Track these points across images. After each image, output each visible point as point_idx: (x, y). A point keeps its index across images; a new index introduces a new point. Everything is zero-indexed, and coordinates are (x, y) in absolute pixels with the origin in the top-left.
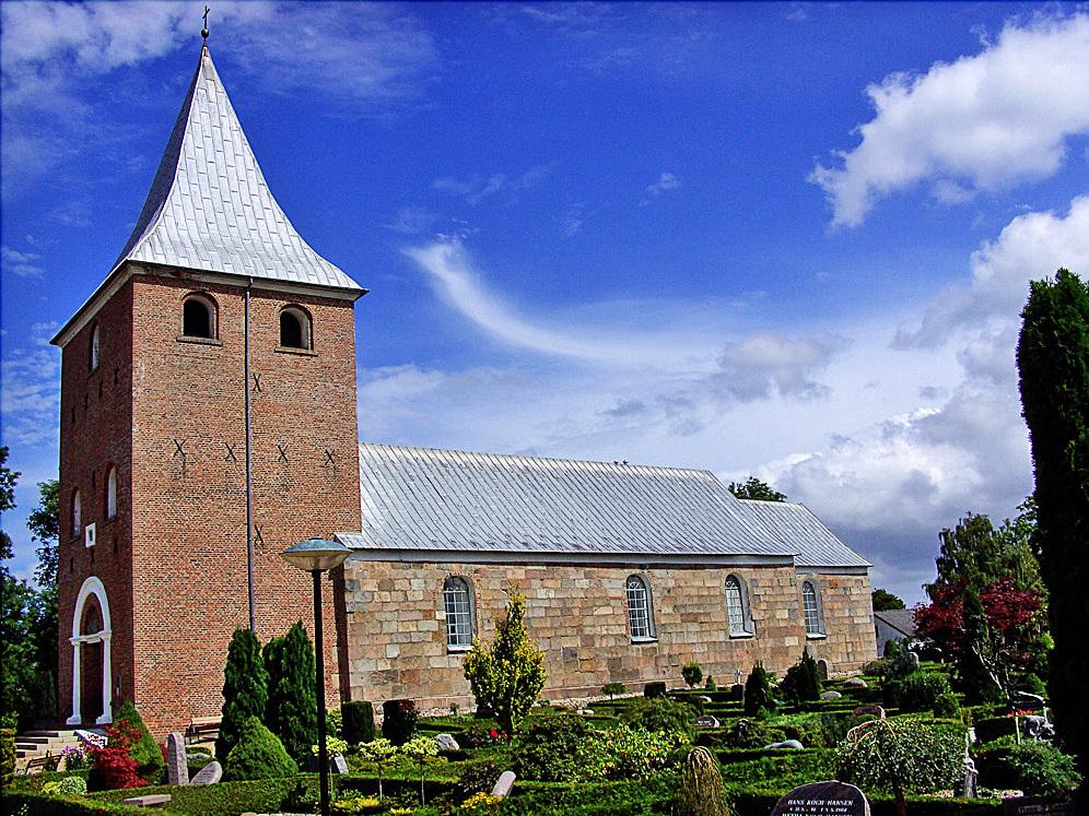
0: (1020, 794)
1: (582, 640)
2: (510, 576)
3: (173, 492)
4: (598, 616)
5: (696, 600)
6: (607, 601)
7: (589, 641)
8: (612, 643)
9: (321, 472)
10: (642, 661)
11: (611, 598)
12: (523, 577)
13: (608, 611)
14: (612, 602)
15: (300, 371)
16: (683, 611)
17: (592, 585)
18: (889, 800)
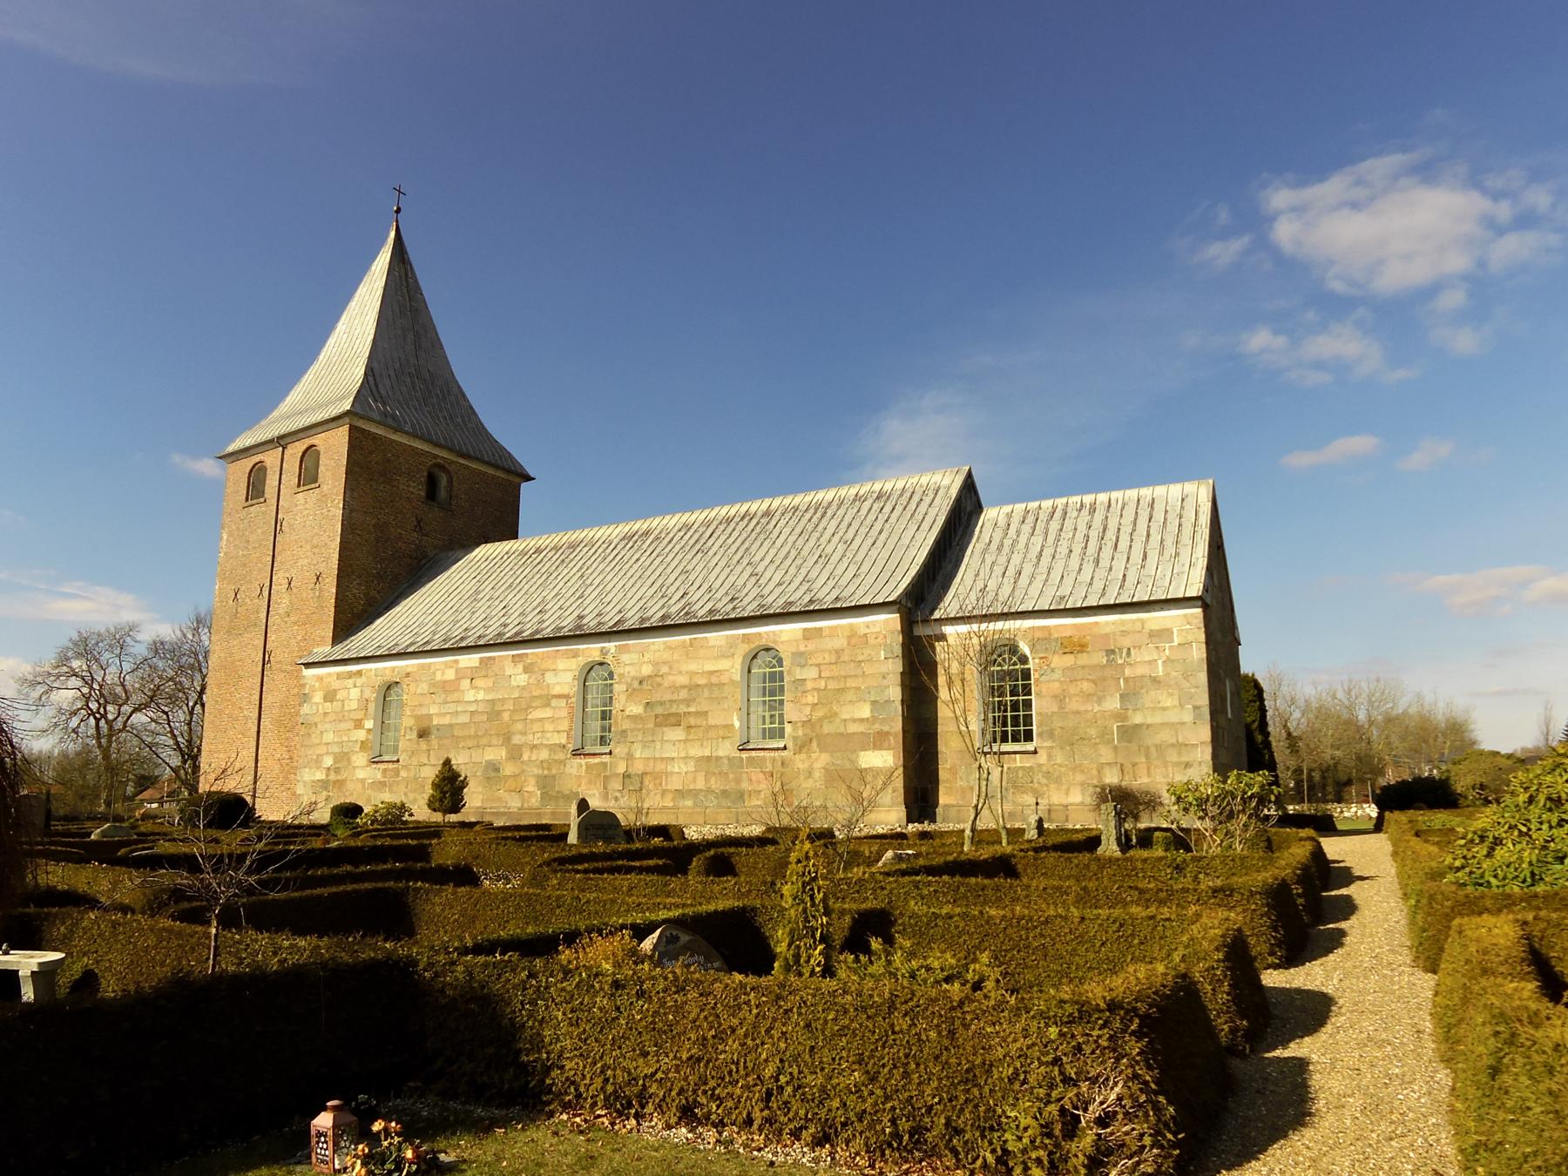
1: (508, 752)
5: (683, 694)
6: (547, 700)
12: (453, 677)
13: (547, 713)
14: (554, 702)
16: (659, 710)
17: (531, 681)
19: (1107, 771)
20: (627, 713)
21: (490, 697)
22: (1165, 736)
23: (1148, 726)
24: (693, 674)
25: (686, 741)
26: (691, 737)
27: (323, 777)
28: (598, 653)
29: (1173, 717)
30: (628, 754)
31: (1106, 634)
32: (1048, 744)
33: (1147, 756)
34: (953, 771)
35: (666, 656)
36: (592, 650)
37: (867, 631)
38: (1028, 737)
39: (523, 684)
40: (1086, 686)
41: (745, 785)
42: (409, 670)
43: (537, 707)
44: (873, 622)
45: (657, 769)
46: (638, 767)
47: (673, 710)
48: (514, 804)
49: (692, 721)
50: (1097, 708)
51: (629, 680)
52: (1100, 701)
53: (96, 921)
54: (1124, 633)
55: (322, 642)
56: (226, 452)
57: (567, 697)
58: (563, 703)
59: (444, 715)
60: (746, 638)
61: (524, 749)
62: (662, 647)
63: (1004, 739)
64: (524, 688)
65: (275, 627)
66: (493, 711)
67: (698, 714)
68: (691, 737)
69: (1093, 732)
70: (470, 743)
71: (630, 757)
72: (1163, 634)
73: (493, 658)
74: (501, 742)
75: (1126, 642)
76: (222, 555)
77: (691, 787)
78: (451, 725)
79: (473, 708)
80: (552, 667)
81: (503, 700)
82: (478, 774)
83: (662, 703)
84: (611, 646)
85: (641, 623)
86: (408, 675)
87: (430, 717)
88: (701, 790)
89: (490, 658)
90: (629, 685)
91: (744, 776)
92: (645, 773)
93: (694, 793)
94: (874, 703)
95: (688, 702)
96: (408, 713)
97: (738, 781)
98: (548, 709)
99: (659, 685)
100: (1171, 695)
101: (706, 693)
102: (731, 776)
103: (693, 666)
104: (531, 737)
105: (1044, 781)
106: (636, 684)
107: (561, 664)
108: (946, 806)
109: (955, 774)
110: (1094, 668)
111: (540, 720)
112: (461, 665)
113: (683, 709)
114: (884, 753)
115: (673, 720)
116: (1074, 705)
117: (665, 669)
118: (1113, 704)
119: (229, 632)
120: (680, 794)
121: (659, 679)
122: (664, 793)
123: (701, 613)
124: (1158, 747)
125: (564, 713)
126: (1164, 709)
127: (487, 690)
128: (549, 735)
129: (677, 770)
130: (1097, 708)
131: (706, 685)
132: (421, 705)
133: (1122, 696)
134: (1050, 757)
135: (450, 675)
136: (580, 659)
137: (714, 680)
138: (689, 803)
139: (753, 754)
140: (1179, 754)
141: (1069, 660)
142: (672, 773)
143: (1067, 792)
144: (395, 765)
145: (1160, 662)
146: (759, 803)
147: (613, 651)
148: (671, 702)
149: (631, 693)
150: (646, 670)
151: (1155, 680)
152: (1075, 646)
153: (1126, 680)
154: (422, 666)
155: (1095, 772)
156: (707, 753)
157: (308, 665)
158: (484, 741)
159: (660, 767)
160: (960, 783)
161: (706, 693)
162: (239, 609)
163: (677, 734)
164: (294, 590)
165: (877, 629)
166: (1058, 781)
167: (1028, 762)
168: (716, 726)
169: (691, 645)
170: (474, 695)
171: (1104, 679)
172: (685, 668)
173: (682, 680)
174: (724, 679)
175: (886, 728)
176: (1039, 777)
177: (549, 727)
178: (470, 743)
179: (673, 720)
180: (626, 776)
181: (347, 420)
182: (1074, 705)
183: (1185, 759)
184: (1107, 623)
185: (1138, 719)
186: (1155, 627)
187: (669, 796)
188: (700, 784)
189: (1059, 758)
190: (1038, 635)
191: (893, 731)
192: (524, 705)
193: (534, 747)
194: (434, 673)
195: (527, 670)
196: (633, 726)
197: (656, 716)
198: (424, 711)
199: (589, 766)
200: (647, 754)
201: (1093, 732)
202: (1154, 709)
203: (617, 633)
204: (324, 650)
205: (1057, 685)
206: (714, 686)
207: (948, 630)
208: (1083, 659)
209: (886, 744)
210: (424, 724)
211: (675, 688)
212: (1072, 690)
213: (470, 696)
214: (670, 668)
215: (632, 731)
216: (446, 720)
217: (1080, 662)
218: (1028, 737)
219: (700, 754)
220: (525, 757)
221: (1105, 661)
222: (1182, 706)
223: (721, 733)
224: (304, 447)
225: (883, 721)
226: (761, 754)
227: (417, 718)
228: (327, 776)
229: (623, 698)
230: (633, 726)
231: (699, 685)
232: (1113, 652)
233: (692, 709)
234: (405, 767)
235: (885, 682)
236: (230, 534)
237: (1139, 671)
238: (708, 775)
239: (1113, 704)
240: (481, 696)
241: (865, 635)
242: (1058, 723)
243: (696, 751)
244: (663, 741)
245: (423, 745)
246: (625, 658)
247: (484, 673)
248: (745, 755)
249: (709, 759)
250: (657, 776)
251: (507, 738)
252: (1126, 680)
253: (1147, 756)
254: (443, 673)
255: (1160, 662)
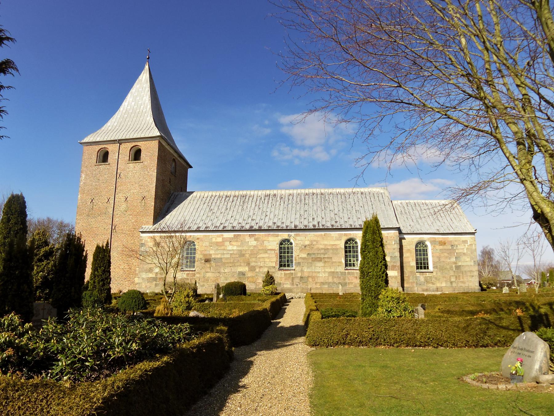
0: (477, 5)
1: (249, 268)
2: (214, 240)
3: (88, 215)
4: (259, 258)
5: (322, 251)
6: (266, 251)
7: (252, 269)
8: (228, 256)
9: (139, 204)
10: (283, 279)
11: (268, 250)
12: (221, 241)
13: (267, 255)
14: (269, 252)
15: (135, 169)
16: (313, 256)
17: (258, 244)
18: (167, 363)
19: (452, 277)
20: (300, 256)
21: (240, 249)
22: (467, 269)
23: (463, 266)
24: (326, 245)
25: (324, 266)
26: (326, 265)
27: (154, 276)
28: (287, 236)
29: (469, 264)
30: (302, 270)
31: (451, 241)
32: (436, 270)
33: (463, 273)
34: (409, 277)
35: (315, 238)
36: (284, 235)
37: (388, 235)
38: (194, 267)
39: (254, 245)
40: (446, 254)
41: (347, 281)
42: (198, 237)
43: (261, 253)
44: (390, 233)
45: (313, 275)
46: (306, 275)
47: (319, 256)
48: (252, 287)
49: (326, 260)
50: (449, 261)
51: (300, 246)
52: (450, 258)
53: (68, 339)
54: (456, 241)
55: (147, 223)
56: (82, 142)
57: (274, 250)
58: (273, 252)
59: (218, 254)
60: (345, 235)
61: (256, 268)
62: (313, 236)
63: (421, 268)
64: (255, 246)
65: (118, 216)
66: (241, 254)
67: (328, 258)
68: (326, 265)
69: (448, 267)
70: (231, 265)
71: (302, 271)
72: (465, 242)
73: (240, 235)
74: (245, 265)
75: (456, 243)
76: (82, 183)
77: (327, 281)
78: (221, 258)
79: (232, 252)
80: (267, 239)
81: (246, 251)
82: (235, 276)
83: (314, 254)
84: (293, 234)
85: (223, 229)
86: (198, 239)
87: (211, 255)
88: (330, 282)
89: (239, 235)
90: (300, 248)
91: (347, 278)
92: (309, 277)
93: (329, 283)
94: (391, 257)
95: (324, 254)
96: (199, 253)
97: (344, 279)
98: (266, 254)
99: (313, 248)
100: (468, 258)
101: (331, 251)
102: (342, 278)
103: (326, 243)
104: (259, 263)
105: (435, 280)
106: (303, 247)
107: (271, 239)
108: (408, 288)
109: (409, 278)
110: (448, 249)
111: (263, 258)
112: (224, 236)
113: (322, 256)
114: (394, 271)
115: (320, 260)
116: (442, 259)
117: (314, 243)
118: (453, 259)
119: (88, 215)
120: (322, 283)
121: (313, 246)
122: (316, 283)
123: (329, 225)
124: (465, 271)
125: (274, 256)
126: (467, 261)
127: (237, 246)
128: (267, 263)
129: (321, 276)
130: (449, 261)
131: (331, 249)
132: (205, 250)
133: (456, 257)
134: (437, 273)
135: (220, 240)
136: (279, 237)
137: (334, 247)
138: (326, 286)
139: (350, 271)
140: (471, 273)
141: (441, 247)
142: (319, 277)
143: (441, 283)
144: (193, 272)
145: (465, 249)
146: (352, 286)
147: (293, 235)
148: (318, 253)
149: (301, 250)
150: (307, 243)
151: (464, 254)
152: (443, 243)
153: (457, 253)
154: (206, 236)
155: (449, 278)
156: (333, 270)
157: (142, 232)
158: (236, 264)
159: (314, 275)
160: (410, 281)
161: (331, 251)
162: (94, 207)
163: (321, 264)
164: (129, 202)
165: (391, 235)
166: (439, 280)
167: (431, 275)
168: (336, 262)
169: (324, 236)
170: (233, 247)
171: (451, 253)
172: (322, 243)
173: (321, 247)
174: (338, 247)
175: (395, 264)
176: (433, 279)
177: (267, 260)
178: (231, 265)
179: (319, 259)
180: (301, 277)
181: (158, 138)
182: (442, 259)
183: (472, 274)
184: (451, 238)
185: (460, 264)
186: (464, 239)
187: (319, 284)
188: (330, 280)
189: (439, 274)
190: (433, 240)
191: (397, 265)
192: (254, 253)
193: (261, 267)
194: (212, 239)
195: (255, 240)
196: (303, 261)
197: (312, 258)
198: (207, 253)
199: (285, 274)
200: (309, 270)
201: (448, 267)
202: (464, 261)
203: (296, 230)
204: (151, 227)
205: (438, 254)
206: (335, 250)
207: (405, 236)
208: (445, 247)
209: (395, 269)
210: (208, 257)
211: (319, 249)
212: (442, 255)
213: (230, 248)
214: (317, 243)
215: (303, 262)
216: (219, 256)
217: (444, 248)
218: (194, 267)
219: (330, 270)
220: (257, 270)
221: (451, 248)
222: (471, 261)
223: (338, 264)
224: (133, 145)
225: (394, 262)
226: (353, 271)
227: (204, 255)
228: (156, 275)
229: (298, 251)
230: (303, 261)
231: (328, 249)
232: (453, 245)
233: (326, 256)
234: (198, 273)
235: (395, 251)
236: (86, 175)
237: (460, 251)
238: (333, 278)
239: (453, 259)
240: (235, 248)
241: (387, 237)
242: (438, 265)
243: (328, 270)
244: (315, 266)
245: (208, 265)
246: (298, 238)
247: (236, 240)
248: (347, 271)
249: (333, 272)
250: (313, 278)
251: (248, 264)
252: (457, 253)
253: (463, 273)
254: (216, 239)
255: (465, 249)
